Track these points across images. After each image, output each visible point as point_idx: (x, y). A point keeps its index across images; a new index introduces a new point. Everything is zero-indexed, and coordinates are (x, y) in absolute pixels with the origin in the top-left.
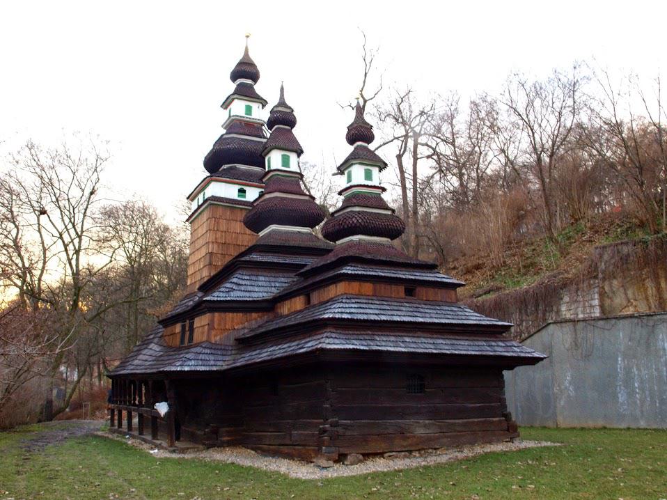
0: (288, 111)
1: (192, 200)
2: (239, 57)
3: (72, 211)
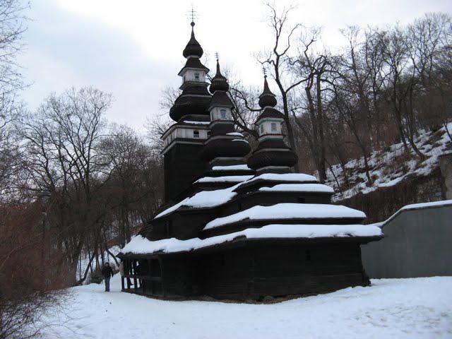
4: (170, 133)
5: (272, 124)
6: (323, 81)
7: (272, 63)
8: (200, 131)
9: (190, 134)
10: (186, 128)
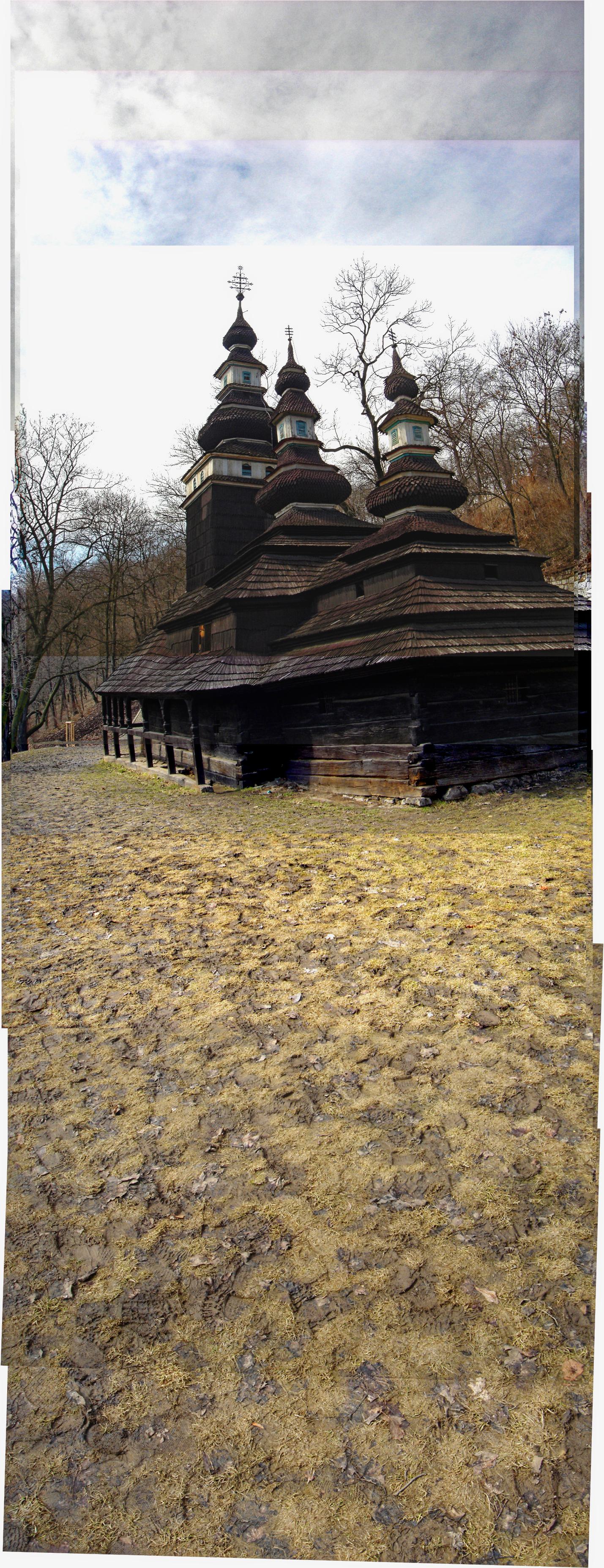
0: (299, 371)
1: (187, 482)
3: (44, 501)
4: (200, 469)
5: (415, 428)
7: (357, 375)
8: (253, 465)
9: (237, 469)
10: (228, 458)
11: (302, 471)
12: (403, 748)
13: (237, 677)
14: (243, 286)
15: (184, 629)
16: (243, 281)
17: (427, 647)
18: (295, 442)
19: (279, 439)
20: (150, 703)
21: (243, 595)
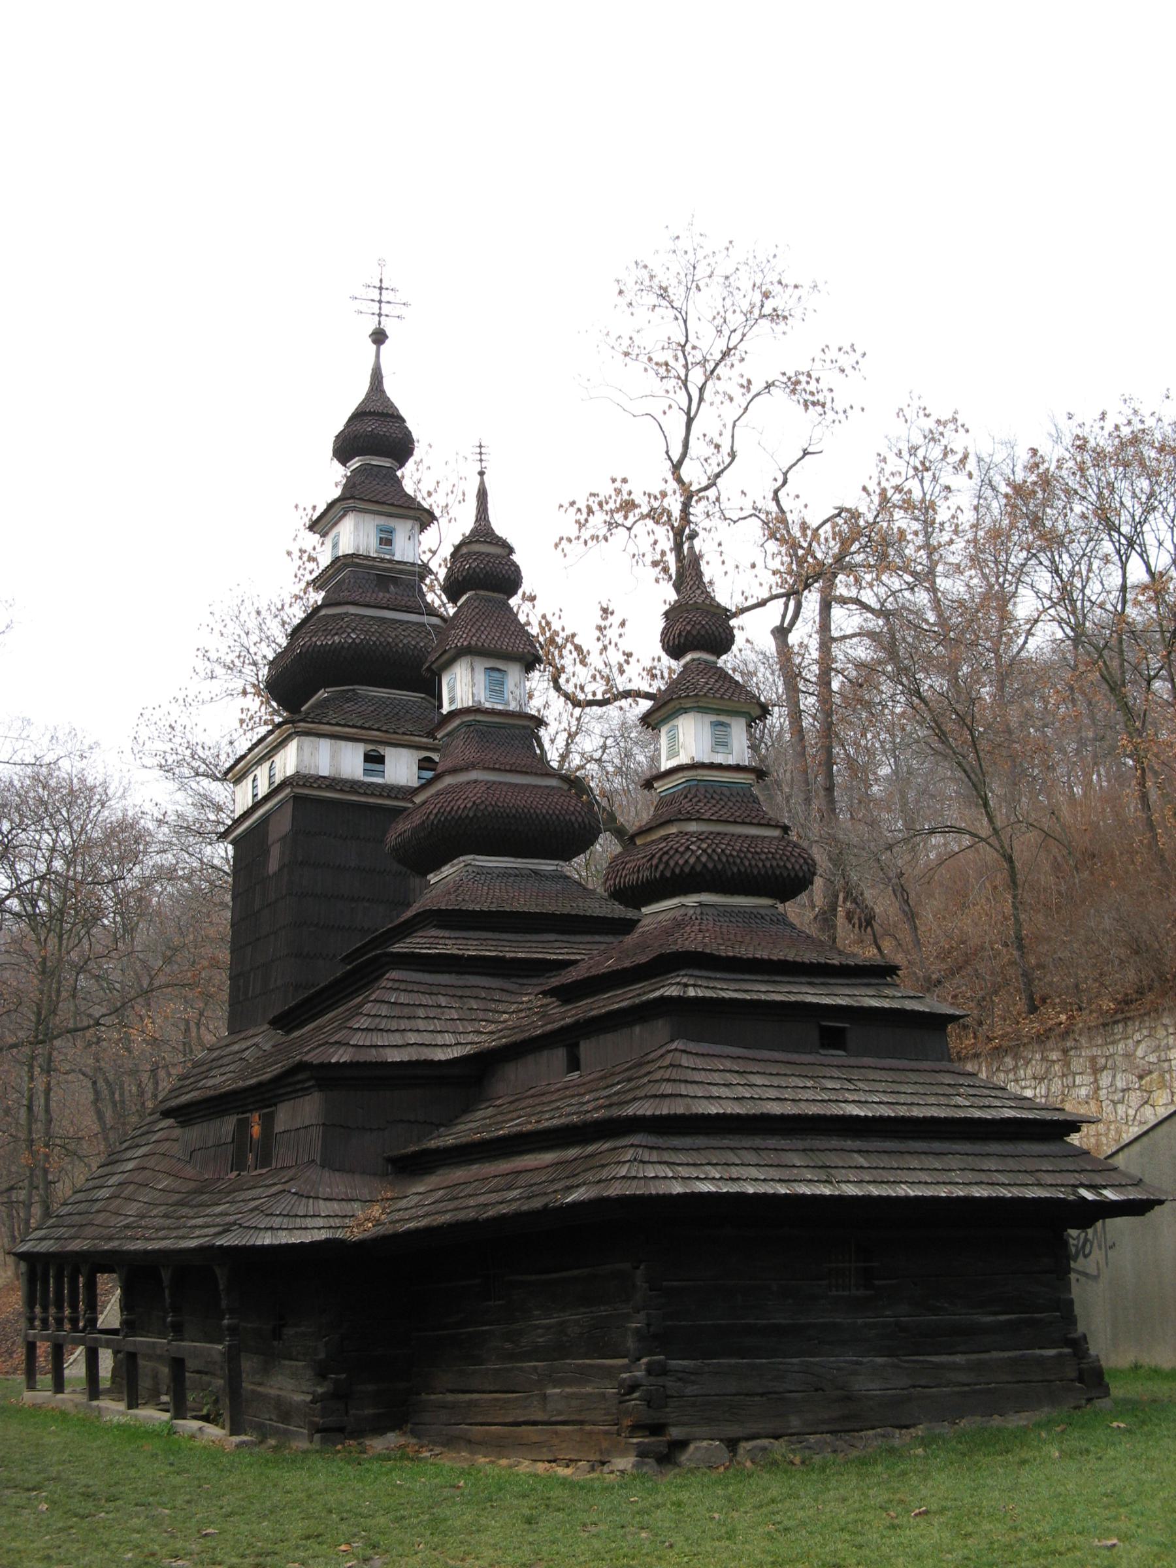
2: (355, 395)
4: (269, 755)
6: (843, 601)
8: (390, 753)
9: (348, 761)
11: (490, 785)
12: (612, 1366)
13: (320, 1222)
14: (386, 309)
15: (226, 1115)
16: (386, 296)
17: (656, 1177)
18: (479, 718)
19: (446, 709)
20: (144, 1277)
21: (341, 1056)
